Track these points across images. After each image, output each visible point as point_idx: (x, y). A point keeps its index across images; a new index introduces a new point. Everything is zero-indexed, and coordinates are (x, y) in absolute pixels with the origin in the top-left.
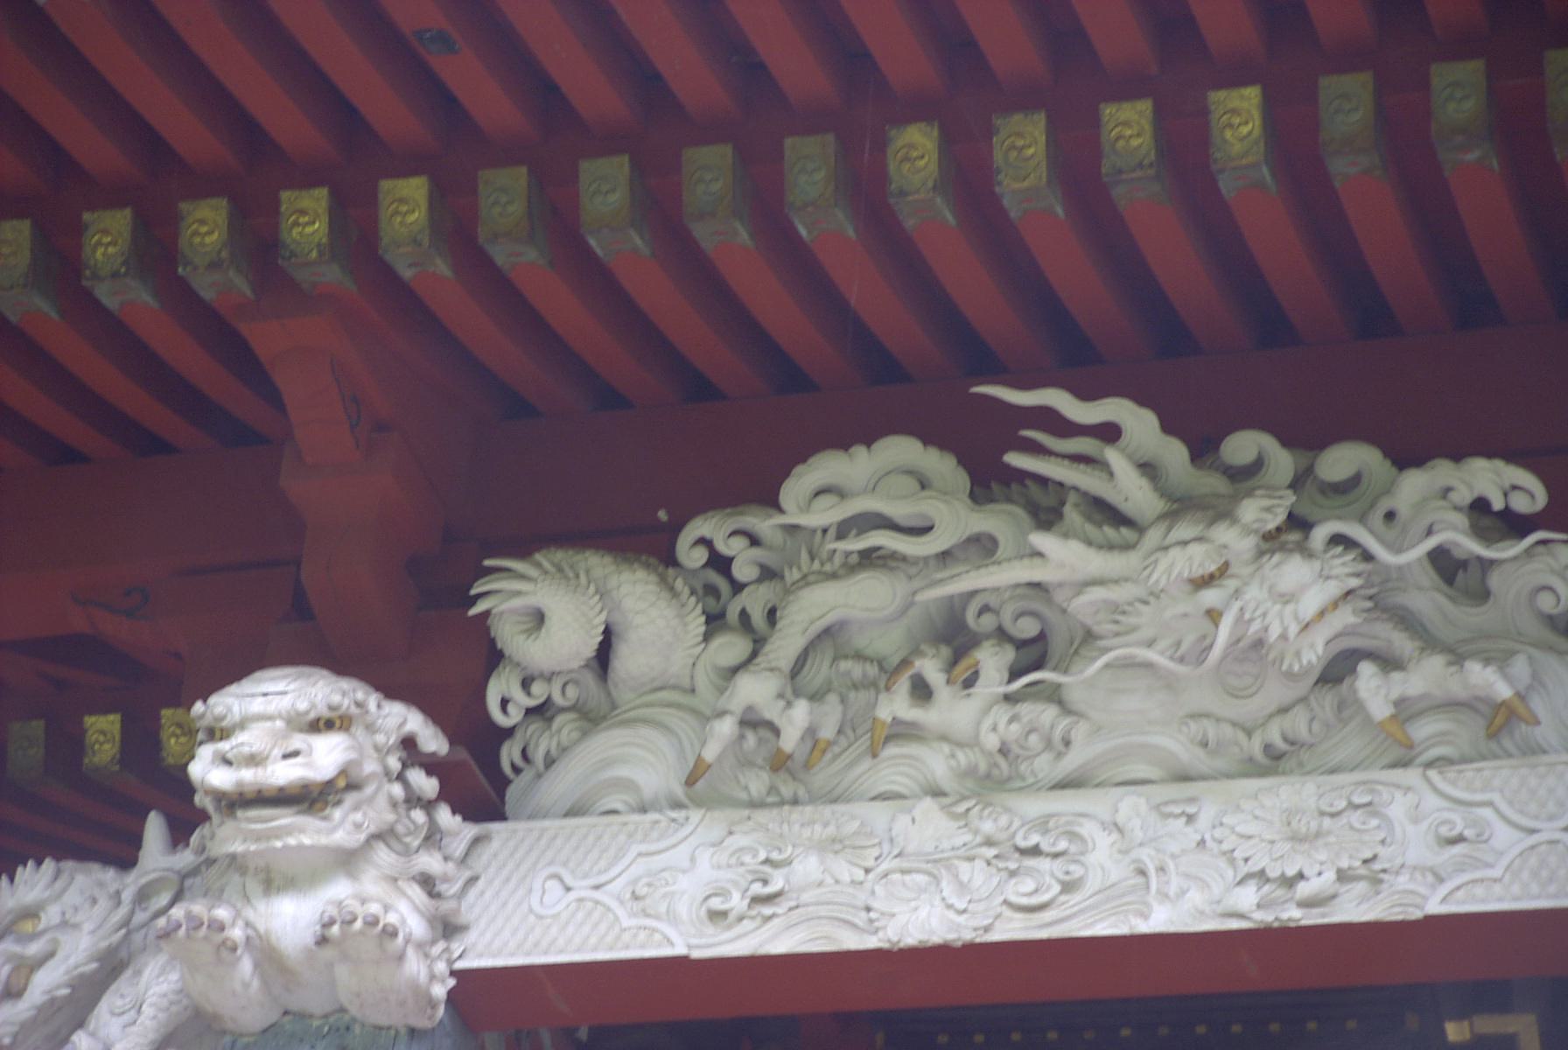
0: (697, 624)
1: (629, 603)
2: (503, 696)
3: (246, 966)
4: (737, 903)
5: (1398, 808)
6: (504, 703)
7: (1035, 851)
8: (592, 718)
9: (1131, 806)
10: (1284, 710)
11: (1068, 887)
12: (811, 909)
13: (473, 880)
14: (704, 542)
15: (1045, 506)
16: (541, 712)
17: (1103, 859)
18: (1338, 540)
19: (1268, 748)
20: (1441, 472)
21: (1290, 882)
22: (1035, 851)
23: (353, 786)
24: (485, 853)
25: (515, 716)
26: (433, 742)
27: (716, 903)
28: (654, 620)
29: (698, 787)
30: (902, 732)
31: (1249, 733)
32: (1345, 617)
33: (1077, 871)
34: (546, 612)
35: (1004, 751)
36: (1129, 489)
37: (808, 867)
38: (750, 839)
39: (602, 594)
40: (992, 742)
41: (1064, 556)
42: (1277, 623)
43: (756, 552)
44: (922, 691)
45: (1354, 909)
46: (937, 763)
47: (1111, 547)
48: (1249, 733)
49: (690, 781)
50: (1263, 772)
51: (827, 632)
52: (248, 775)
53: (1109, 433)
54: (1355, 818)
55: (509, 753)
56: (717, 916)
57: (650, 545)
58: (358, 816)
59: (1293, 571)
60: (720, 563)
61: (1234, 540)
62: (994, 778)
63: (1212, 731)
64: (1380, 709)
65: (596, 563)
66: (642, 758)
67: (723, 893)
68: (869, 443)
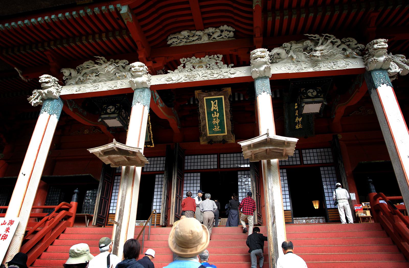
0: (77, 73)
1: (72, 71)
2: (64, 78)
3: (44, 94)
4: (77, 90)
5: (118, 83)
6: (64, 78)
7: (96, 86)
8: (70, 79)
9: (102, 83)
10: (112, 77)
11: (98, 88)
12: (263, 152)
13: (62, 90)
14: (78, 68)
15: (97, 63)
16: (67, 79)
17: (100, 87)
18: (114, 65)
19: (111, 79)
20: (122, 61)
21: (111, 87)
22: (96, 86)
23: (50, 82)
24: (63, 88)
25: (65, 79)
26: (57, 80)
27: (76, 90)
28: (74, 73)
29: (77, 83)
30: (89, 79)
31: (110, 78)
32: (114, 70)
33: (98, 87)
34: (66, 72)
35: (95, 80)
36: (102, 62)
37: (82, 88)
38: (79, 86)
39: (70, 71)
40: (94, 79)
41: (97, 66)
42: (110, 70)
43: (81, 68)
44: (90, 76)
45: (115, 88)
46: (91, 81)
47: (101, 66)
48: (110, 78)
49: (76, 83)
50: (111, 81)
51: (86, 73)
52: (42, 81)
53: (102, 59)
54: (116, 83)
55: (65, 82)
56: (76, 91)
57: (74, 68)
58: (51, 84)
59: (111, 66)
60: (79, 69)
61: (107, 65)
62: (95, 81)
63: (108, 78)
64: (118, 76)
65: (70, 69)
66: (72, 81)
67: (77, 90)
68: (88, 61)
